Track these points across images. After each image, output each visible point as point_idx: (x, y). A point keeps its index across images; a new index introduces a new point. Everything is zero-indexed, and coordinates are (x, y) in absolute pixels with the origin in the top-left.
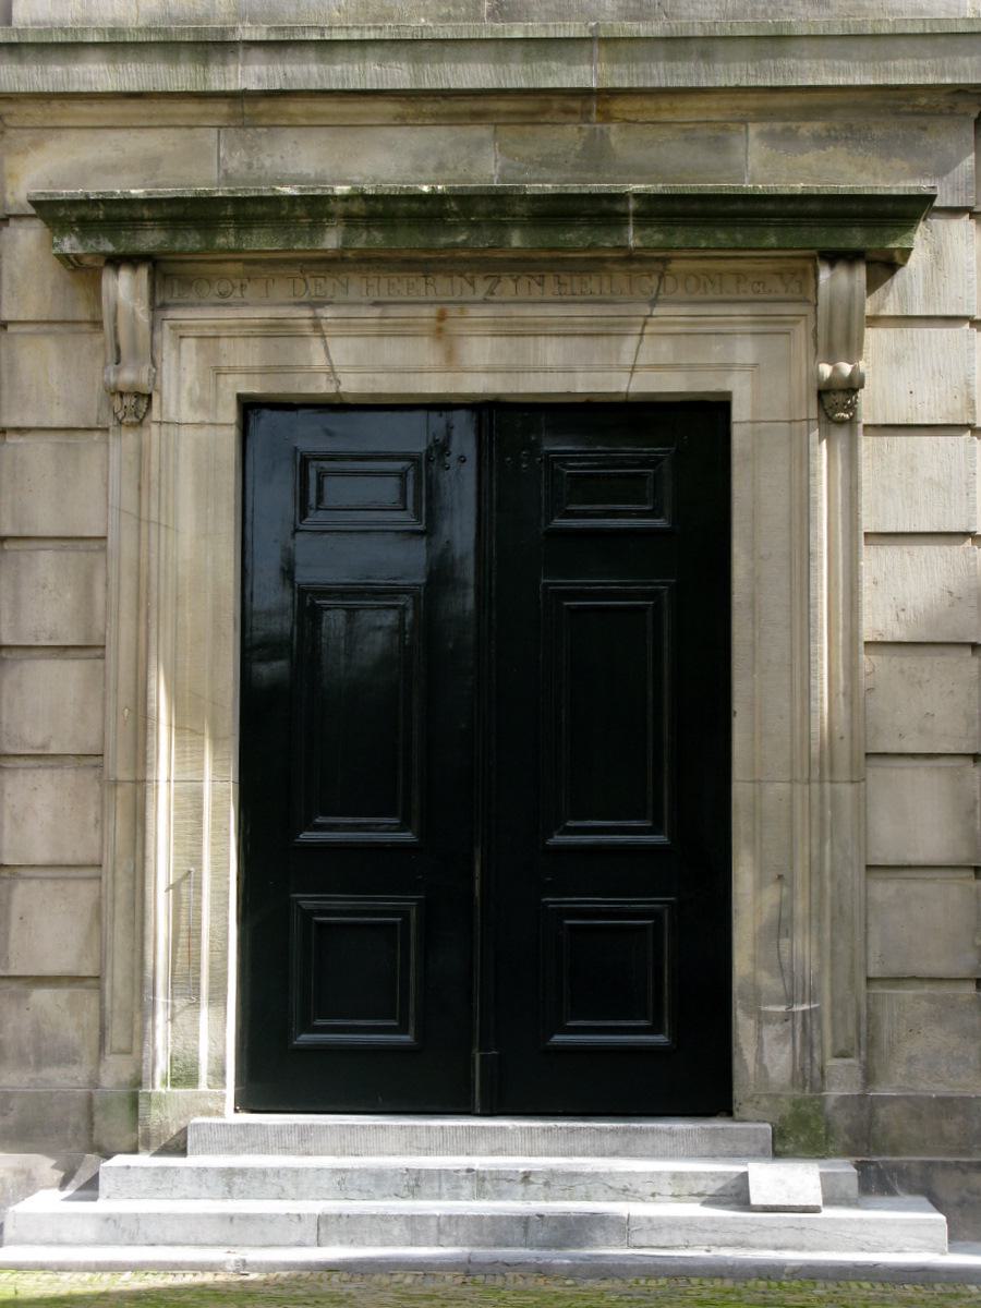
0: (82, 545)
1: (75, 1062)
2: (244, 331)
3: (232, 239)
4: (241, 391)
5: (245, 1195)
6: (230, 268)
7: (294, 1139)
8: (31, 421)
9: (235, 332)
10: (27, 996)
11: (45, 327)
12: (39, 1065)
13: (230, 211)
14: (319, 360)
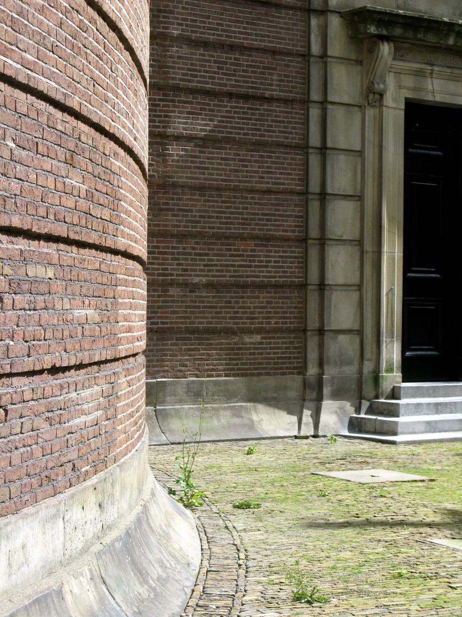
0: (352, 153)
1: (352, 364)
2: (409, 72)
3: (422, 35)
4: (407, 96)
5: (441, 412)
6: (406, 45)
7: (431, 391)
8: (337, 100)
9: (407, 72)
10: (337, 338)
11: (340, 61)
12: (341, 365)
13: (425, 24)
14: (430, 87)
